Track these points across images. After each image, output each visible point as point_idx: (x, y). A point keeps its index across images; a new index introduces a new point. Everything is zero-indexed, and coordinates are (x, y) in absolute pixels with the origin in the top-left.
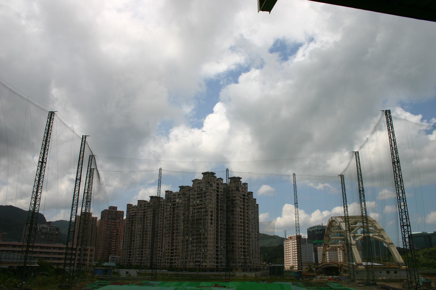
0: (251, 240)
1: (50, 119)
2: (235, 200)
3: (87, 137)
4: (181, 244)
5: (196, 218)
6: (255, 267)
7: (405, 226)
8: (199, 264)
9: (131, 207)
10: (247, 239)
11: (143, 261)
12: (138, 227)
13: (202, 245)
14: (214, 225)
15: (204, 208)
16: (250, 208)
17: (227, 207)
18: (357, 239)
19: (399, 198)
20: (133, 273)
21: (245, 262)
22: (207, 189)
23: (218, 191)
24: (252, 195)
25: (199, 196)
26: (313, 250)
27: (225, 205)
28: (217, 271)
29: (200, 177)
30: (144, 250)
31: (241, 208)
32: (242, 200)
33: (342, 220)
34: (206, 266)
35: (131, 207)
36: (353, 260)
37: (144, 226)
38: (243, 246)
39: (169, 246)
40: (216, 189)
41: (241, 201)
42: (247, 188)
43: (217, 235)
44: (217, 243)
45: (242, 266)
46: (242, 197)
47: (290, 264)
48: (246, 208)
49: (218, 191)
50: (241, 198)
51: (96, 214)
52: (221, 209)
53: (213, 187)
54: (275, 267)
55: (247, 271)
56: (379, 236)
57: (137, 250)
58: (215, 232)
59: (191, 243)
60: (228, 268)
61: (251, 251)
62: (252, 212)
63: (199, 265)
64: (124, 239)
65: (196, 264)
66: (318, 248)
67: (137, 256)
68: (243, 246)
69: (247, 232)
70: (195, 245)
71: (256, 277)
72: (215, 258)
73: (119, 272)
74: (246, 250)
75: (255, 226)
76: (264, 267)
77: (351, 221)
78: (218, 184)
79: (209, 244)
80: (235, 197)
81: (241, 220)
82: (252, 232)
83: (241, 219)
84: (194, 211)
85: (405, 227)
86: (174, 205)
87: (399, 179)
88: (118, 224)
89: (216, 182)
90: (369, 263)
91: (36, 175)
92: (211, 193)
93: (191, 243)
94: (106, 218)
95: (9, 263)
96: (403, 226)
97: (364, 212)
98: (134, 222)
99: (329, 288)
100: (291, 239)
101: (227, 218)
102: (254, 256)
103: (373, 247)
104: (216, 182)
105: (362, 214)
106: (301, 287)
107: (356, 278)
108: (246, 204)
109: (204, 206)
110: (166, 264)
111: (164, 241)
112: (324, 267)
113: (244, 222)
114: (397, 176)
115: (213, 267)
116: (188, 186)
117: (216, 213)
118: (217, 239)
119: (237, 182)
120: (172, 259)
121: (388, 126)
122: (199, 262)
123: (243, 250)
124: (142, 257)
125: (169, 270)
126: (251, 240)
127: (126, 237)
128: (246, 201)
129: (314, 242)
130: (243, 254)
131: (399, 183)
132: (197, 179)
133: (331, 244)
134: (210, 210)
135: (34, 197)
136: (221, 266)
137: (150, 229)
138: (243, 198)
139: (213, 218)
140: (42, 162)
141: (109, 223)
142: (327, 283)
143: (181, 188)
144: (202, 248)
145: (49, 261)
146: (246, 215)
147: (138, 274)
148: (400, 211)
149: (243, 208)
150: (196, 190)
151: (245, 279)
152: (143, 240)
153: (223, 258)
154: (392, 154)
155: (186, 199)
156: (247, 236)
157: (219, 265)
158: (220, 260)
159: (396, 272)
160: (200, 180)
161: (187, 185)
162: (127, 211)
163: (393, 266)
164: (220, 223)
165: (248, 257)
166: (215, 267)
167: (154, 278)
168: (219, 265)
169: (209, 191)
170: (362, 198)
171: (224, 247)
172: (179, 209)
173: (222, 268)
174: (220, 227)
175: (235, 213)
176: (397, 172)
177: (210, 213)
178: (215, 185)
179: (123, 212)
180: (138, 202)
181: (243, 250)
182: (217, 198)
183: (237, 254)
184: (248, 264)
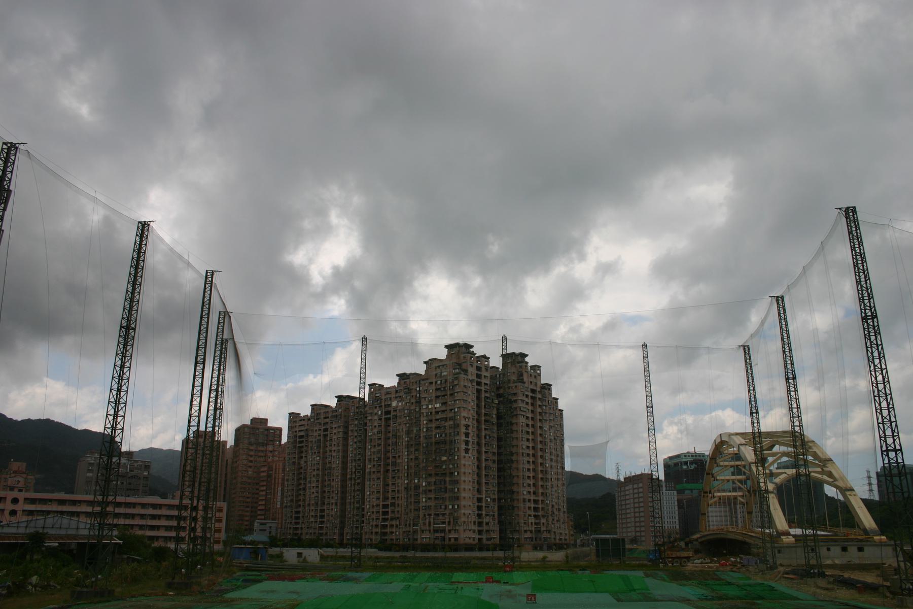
0: (549, 484)
1: (141, 237)
2: (515, 401)
3: (215, 274)
4: (403, 494)
5: (434, 440)
6: (558, 541)
7: (891, 451)
8: (443, 535)
9: (298, 420)
10: (540, 483)
11: (324, 532)
12: (313, 459)
13: (447, 495)
14: (473, 454)
15: (451, 419)
16: (546, 417)
17: (499, 417)
19: (876, 393)
20: (312, 555)
21: (538, 531)
22: (457, 378)
23: (479, 384)
24: (550, 389)
25: (439, 393)
27: (495, 412)
28: (481, 549)
29: (442, 354)
30: (325, 507)
31: (527, 418)
32: (530, 401)
33: (743, 441)
34: (456, 539)
35: (298, 420)
36: (771, 522)
37: (324, 458)
38: (532, 498)
39: (378, 499)
40: (474, 377)
41: (527, 403)
42: (539, 375)
43: (479, 475)
44: (479, 491)
45: (531, 538)
46: (530, 394)
48: (538, 417)
49: (479, 384)
50: (527, 396)
51: (227, 434)
52: (485, 421)
53: (469, 374)
54: (607, 540)
55: (541, 549)
57: (313, 508)
58: (475, 468)
59: (425, 492)
60: (505, 544)
61: (550, 507)
62: (551, 427)
63: (444, 539)
64: (283, 485)
65: (437, 535)
67: (312, 519)
68: (532, 498)
70: (432, 496)
71: (567, 561)
72: (474, 522)
73: (282, 553)
74: (540, 506)
75: (558, 456)
76: (575, 541)
77: (766, 442)
78: (478, 368)
79: (463, 494)
80: (515, 394)
81: (527, 444)
83: (528, 440)
84: (429, 426)
85: (892, 455)
86: (388, 413)
87: (876, 354)
88: (270, 454)
89: (475, 364)
91: (117, 354)
92: (465, 386)
93: (425, 492)
94: (246, 441)
95: (61, 537)
96: (887, 451)
97: (797, 423)
98: (304, 450)
101: (499, 439)
102: (556, 519)
103: (807, 493)
104: (475, 364)
105: (793, 426)
106: (664, 580)
107: (778, 563)
108: (539, 410)
109: (451, 415)
110: (374, 537)
111: (367, 489)
112: (703, 539)
113: (533, 448)
114: (871, 347)
115: (471, 541)
116: (415, 374)
117: (475, 429)
118: (479, 483)
119: (519, 363)
120: (384, 527)
121: (851, 241)
122: (443, 531)
123: (532, 506)
124: (322, 522)
125: (380, 549)
127: (288, 480)
128: (539, 403)
129: (679, 487)
130: (533, 513)
131: (877, 362)
132: (435, 359)
134: (463, 422)
135: (112, 400)
136: (488, 539)
137: (337, 463)
139: (470, 439)
140: (128, 328)
141: (252, 453)
142: (718, 573)
143: (402, 377)
144: (447, 503)
145: (140, 533)
146: (539, 432)
147: (322, 557)
148: (880, 420)
150: (434, 381)
151: (544, 566)
152: (323, 486)
153: (492, 524)
154: (861, 300)
155: (413, 400)
156: (540, 476)
157: (484, 537)
158: (485, 528)
159: (860, 549)
160: (442, 361)
161: (413, 372)
162: (290, 428)
163: (853, 537)
164: (484, 449)
165: (543, 521)
166: (476, 541)
167: (357, 564)
168: (484, 537)
169: (462, 383)
170: (793, 393)
171: (494, 500)
172: (399, 421)
173: (489, 542)
174: (484, 457)
175: (515, 428)
176: (873, 338)
177: (463, 430)
178: (472, 370)
179: (280, 430)
180: (313, 409)
181: (532, 506)
182: (478, 398)
183: (521, 513)
184: (545, 535)
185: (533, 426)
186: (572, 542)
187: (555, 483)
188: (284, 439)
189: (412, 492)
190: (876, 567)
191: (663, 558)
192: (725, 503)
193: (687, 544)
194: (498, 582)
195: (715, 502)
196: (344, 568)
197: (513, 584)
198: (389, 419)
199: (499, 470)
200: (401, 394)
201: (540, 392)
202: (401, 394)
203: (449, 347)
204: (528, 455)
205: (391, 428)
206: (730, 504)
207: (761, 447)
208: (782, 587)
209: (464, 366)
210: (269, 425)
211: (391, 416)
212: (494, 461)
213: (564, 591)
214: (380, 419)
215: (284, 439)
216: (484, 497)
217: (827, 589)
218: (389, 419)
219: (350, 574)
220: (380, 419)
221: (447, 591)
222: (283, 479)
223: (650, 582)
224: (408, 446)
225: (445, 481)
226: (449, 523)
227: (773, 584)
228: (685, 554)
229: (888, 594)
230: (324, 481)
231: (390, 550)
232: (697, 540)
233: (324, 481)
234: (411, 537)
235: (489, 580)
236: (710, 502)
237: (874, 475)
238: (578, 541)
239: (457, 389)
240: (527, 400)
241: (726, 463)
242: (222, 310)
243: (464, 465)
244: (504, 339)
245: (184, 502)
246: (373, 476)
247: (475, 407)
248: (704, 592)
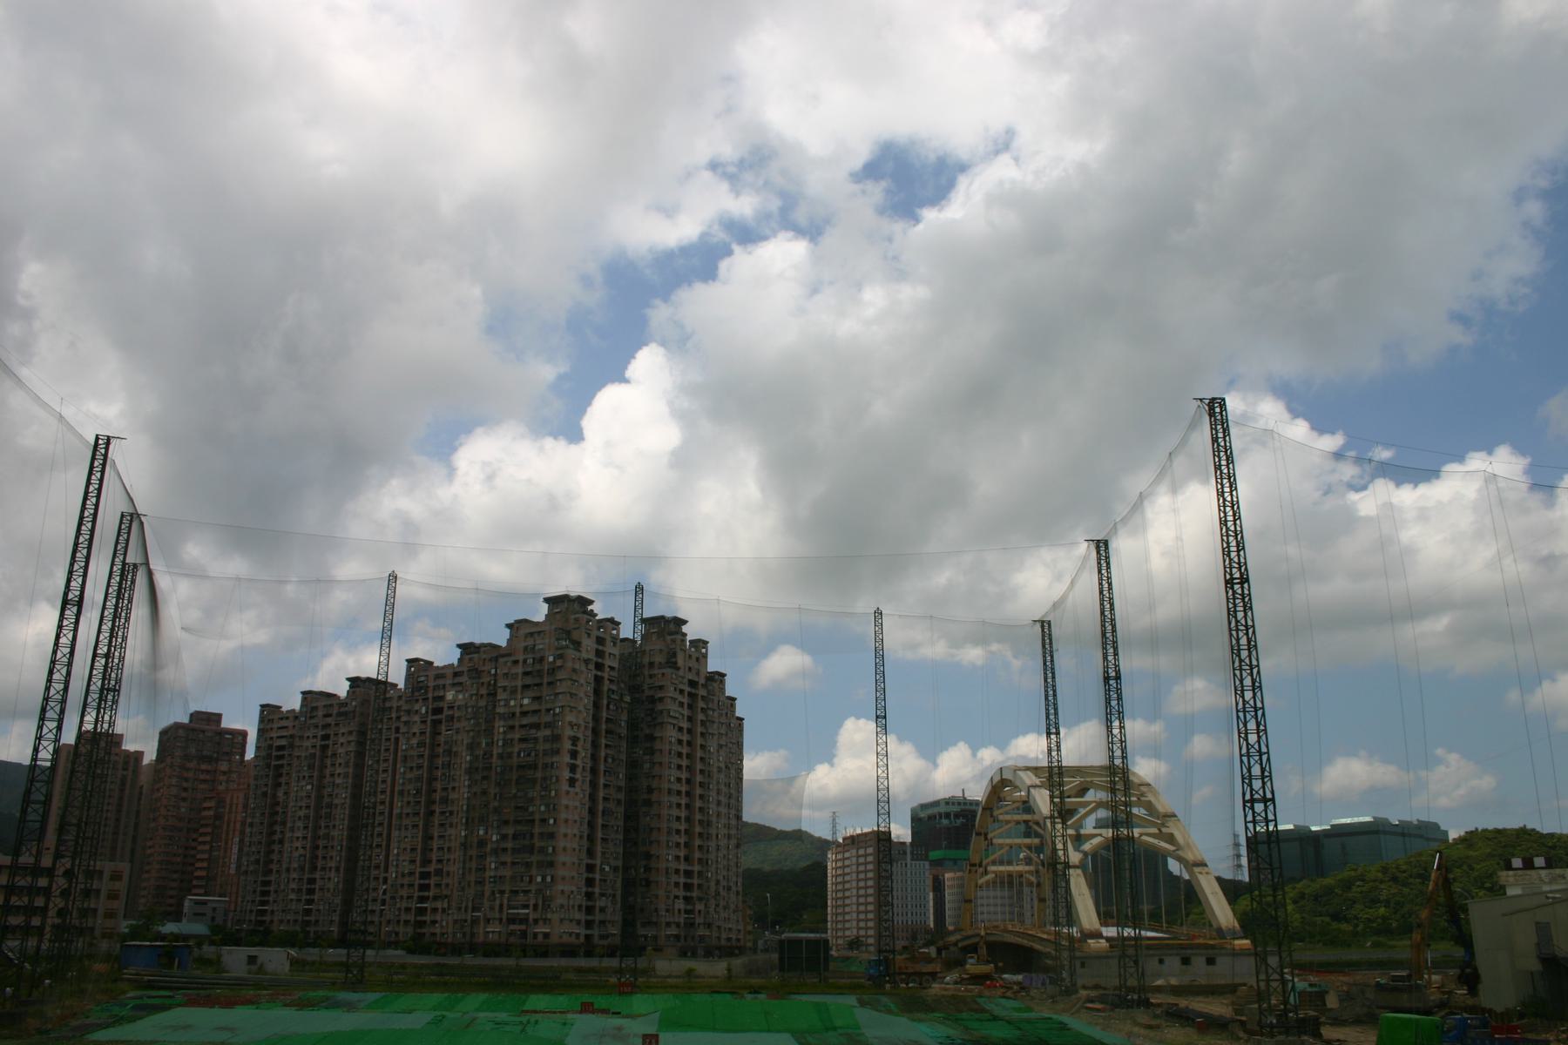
0: (713, 844)
3: (113, 442)
6: (723, 942)
7: (1258, 801)
8: (523, 927)
9: (276, 717)
10: (698, 842)
11: (312, 918)
13: (535, 858)
14: (582, 788)
15: (548, 725)
16: (713, 729)
20: (276, 959)
21: (690, 925)
22: (561, 656)
23: (599, 666)
24: (722, 682)
25: (529, 681)
27: (624, 717)
28: (589, 954)
30: (317, 875)
31: (680, 729)
32: (686, 700)
33: (1038, 782)
34: (546, 935)
35: (276, 717)
36: (1071, 918)
37: (320, 787)
38: (683, 867)
40: (592, 656)
41: (681, 704)
42: (705, 656)
43: (591, 825)
44: (590, 853)
45: (677, 937)
46: (687, 689)
49: (599, 666)
50: (682, 691)
51: (139, 735)
54: (800, 941)
57: (294, 875)
58: (585, 813)
59: (495, 852)
60: (630, 946)
61: (713, 884)
63: (524, 934)
64: (242, 833)
65: (512, 927)
67: (293, 896)
68: (683, 867)
69: (698, 817)
71: (730, 977)
73: (219, 956)
74: (696, 881)
76: (755, 943)
77: (1071, 783)
78: (600, 641)
79: (561, 858)
80: (661, 688)
81: (678, 774)
83: (679, 767)
86: (438, 711)
89: (595, 633)
90: (1128, 932)
92: (574, 670)
93: (495, 852)
96: (1253, 801)
97: (1118, 753)
102: (722, 903)
103: (1137, 873)
104: (595, 633)
105: (1112, 758)
106: (890, 1012)
107: (1080, 982)
108: (701, 717)
109: (548, 718)
110: (401, 929)
111: (394, 844)
113: (688, 781)
115: (573, 940)
116: (490, 645)
117: (589, 745)
118: (591, 838)
119: (671, 634)
120: (422, 911)
122: (524, 920)
123: (682, 880)
124: (310, 902)
125: (411, 951)
126: (713, 844)
127: (251, 825)
128: (701, 704)
130: (682, 893)
132: (526, 621)
133: (994, 863)
134: (569, 732)
136: (602, 937)
137: (343, 797)
138: (690, 694)
139: (579, 762)
142: (979, 1000)
144: (534, 872)
146: (699, 754)
147: (294, 962)
148: (1244, 751)
149: (689, 731)
150: (521, 658)
151: (690, 984)
152: (316, 837)
154: (1226, 552)
155: (483, 691)
157: (596, 932)
158: (598, 917)
159: (1211, 961)
163: (1201, 941)
164: (602, 781)
165: (699, 906)
166: (582, 939)
167: (356, 978)
168: (596, 932)
169: (569, 664)
170: (1114, 703)
171: (615, 869)
174: (601, 794)
175: (658, 745)
176: (1240, 615)
177: (567, 745)
178: (589, 644)
179: (244, 734)
180: (304, 699)
181: (682, 880)
183: (661, 893)
184: (701, 932)
185: (689, 743)
186: (749, 944)
187: (723, 842)
188: (250, 754)
189: (473, 852)
190: (1232, 989)
191: (895, 974)
192: (1002, 883)
193: (939, 951)
194: (605, 1011)
195: (988, 883)
196: (333, 984)
197: (627, 1017)
198: (440, 722)
199: (627, 818)
200: (464, 679)
201: (704, 686)
202: (464, 679)
203: (552, 601)
204: (679, 793)
205: (442, 739)
206: (1011, 884)
207: (1062, 793)
208: (1080, 1024)
209: (575, 635)
210: (225, 724)
211: (443, 717)
212: (619, 802)
213: (714, 1030)
214: (424, 722)
215: (250, 754)
216: (598, 862)
217: (1150, 1027)
218: (440, 722)
219: (343, 996)
220: (424, 722)
221: (508, 1028)
222: (243, 823)
223: (864, 1016)
224: (471, 771)
225: (532, 835)
226: (536, 906)
227: (1065, 1018)
228: (929, 968)
229: (1242, 1034)
230: (317, 827)
231: (429, 953)
232: (956, 944)
233: (317, 827)
234: (467, 930)
235: (587, 1008)
236: (980, 882)
237: (1243, 841)
238: (760, 943)
239: (560, 675)
240: (680, 698)
241: (1008, 817)
242: (127, 509)
243: (567, 807)
244: (639, 589)
245: (22, 860)
246: (406, 822)
247: (591, 706)
248: (951, 1032)
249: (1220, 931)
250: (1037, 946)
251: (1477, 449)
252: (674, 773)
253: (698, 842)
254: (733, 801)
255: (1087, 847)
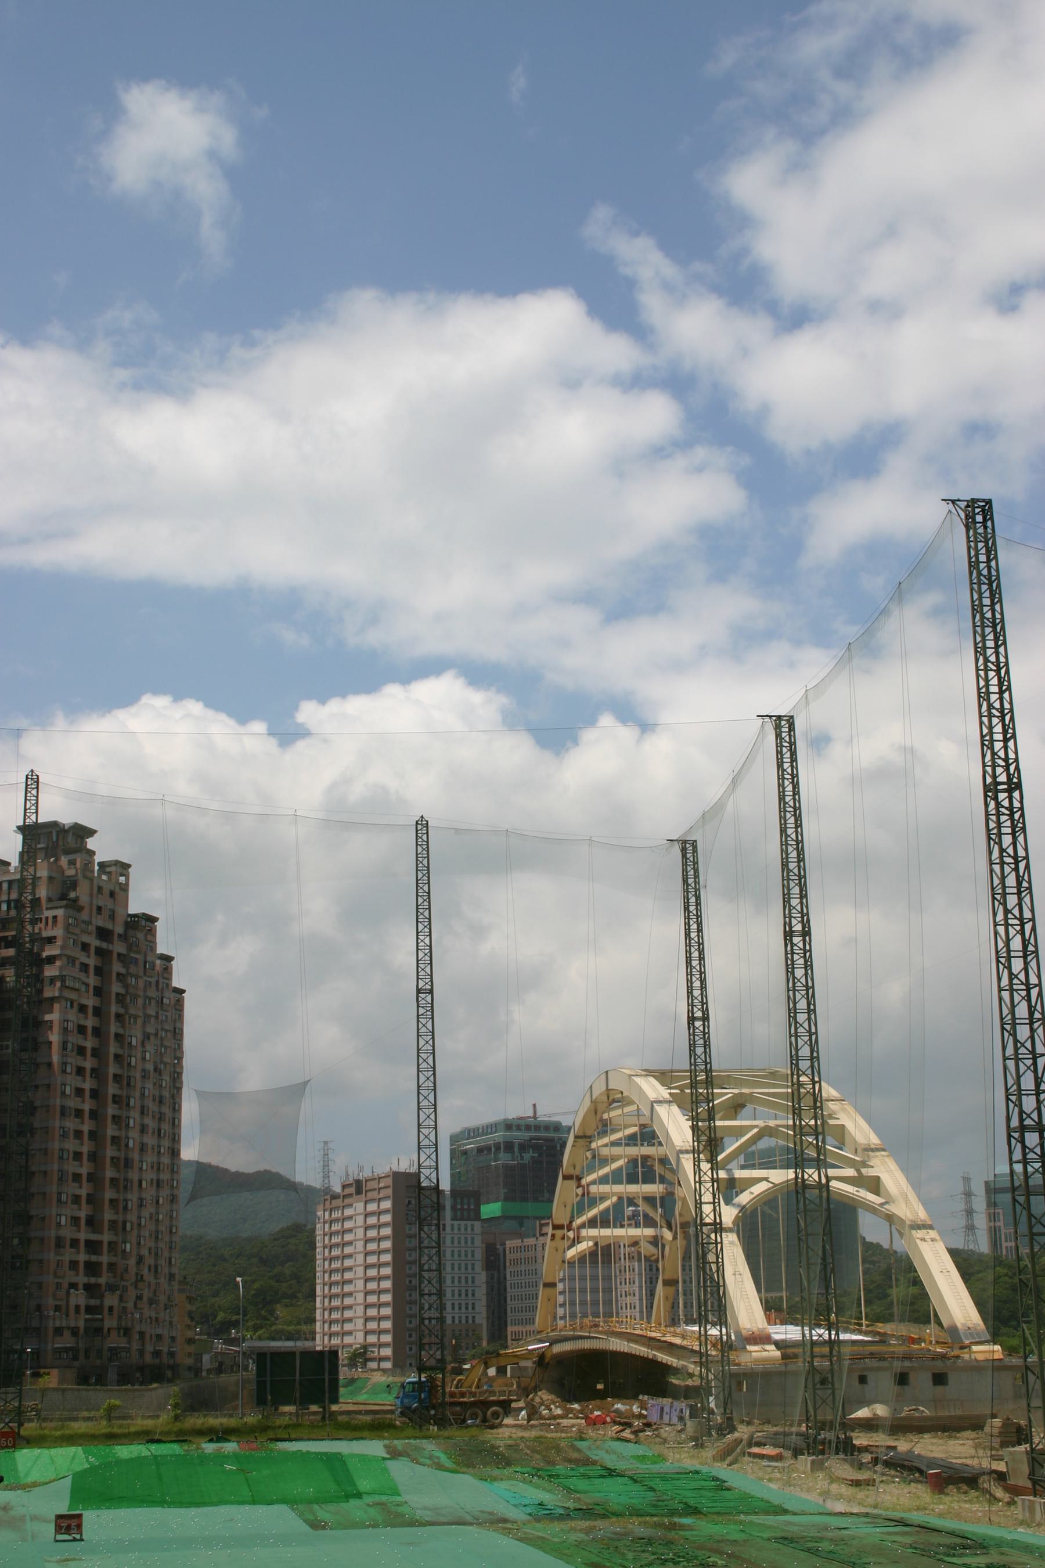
0: (133, 1197)
6: (148, 1359)
7: (1031, 1129)
10: (109, 1194)
18: (744, 1198)
21: (96, 1331)
24: (152, 932)
26: (479, 1254)
31: (83, 1009)
32: (92, 961)
41: (85, 967)
42: (125, 888)
46: (95, 942)
47: (348, 1340)
50: (85, 947)
56: (856, 1181)
61: (132, 1262)
62: (147, 1036)
66: (509, 1244)
68: (83, 1236)
69: (110, 1152)
74: (105, 1259)
75: (161, 1119)
76: (199, 1358)
82: (143, 1148)
83: (80, 1071)
87: (1011, 880)
90: (821, 1333)
96: (1023, 1129)
99: (597, 1470)
100: (359, 1192)
106: (440, 1467)
108: (116, 988)
113: (95, 1094)
119: (67, 852)
123: (82, 1257)
126: (133, 1197)
128: (117, 967)
130: (82, 1279)
133: (592, 1223)
138: (99, 952)
146: (113, 1048)
149: (97, 1012)
181: (82, 1257)
184: (115, 1341)
185: (97, 1032)
187: (149, 1194)
201: (123, 937)
204: (79, 1113)
213: (162, 1503)
217: (857, 1483)
227: (722, 1470)
229: (999, 1493)
249: (953, 1330)
250: (662, 1357)
251: (157, 690)
252: (72, 1081)
253: (109, 1194)
254: (165, 1126)
255: (744, 1198)
